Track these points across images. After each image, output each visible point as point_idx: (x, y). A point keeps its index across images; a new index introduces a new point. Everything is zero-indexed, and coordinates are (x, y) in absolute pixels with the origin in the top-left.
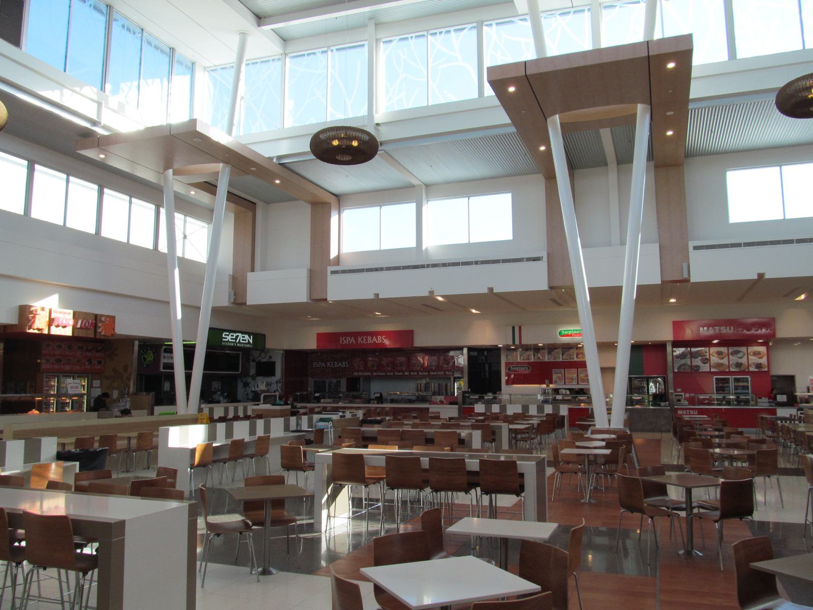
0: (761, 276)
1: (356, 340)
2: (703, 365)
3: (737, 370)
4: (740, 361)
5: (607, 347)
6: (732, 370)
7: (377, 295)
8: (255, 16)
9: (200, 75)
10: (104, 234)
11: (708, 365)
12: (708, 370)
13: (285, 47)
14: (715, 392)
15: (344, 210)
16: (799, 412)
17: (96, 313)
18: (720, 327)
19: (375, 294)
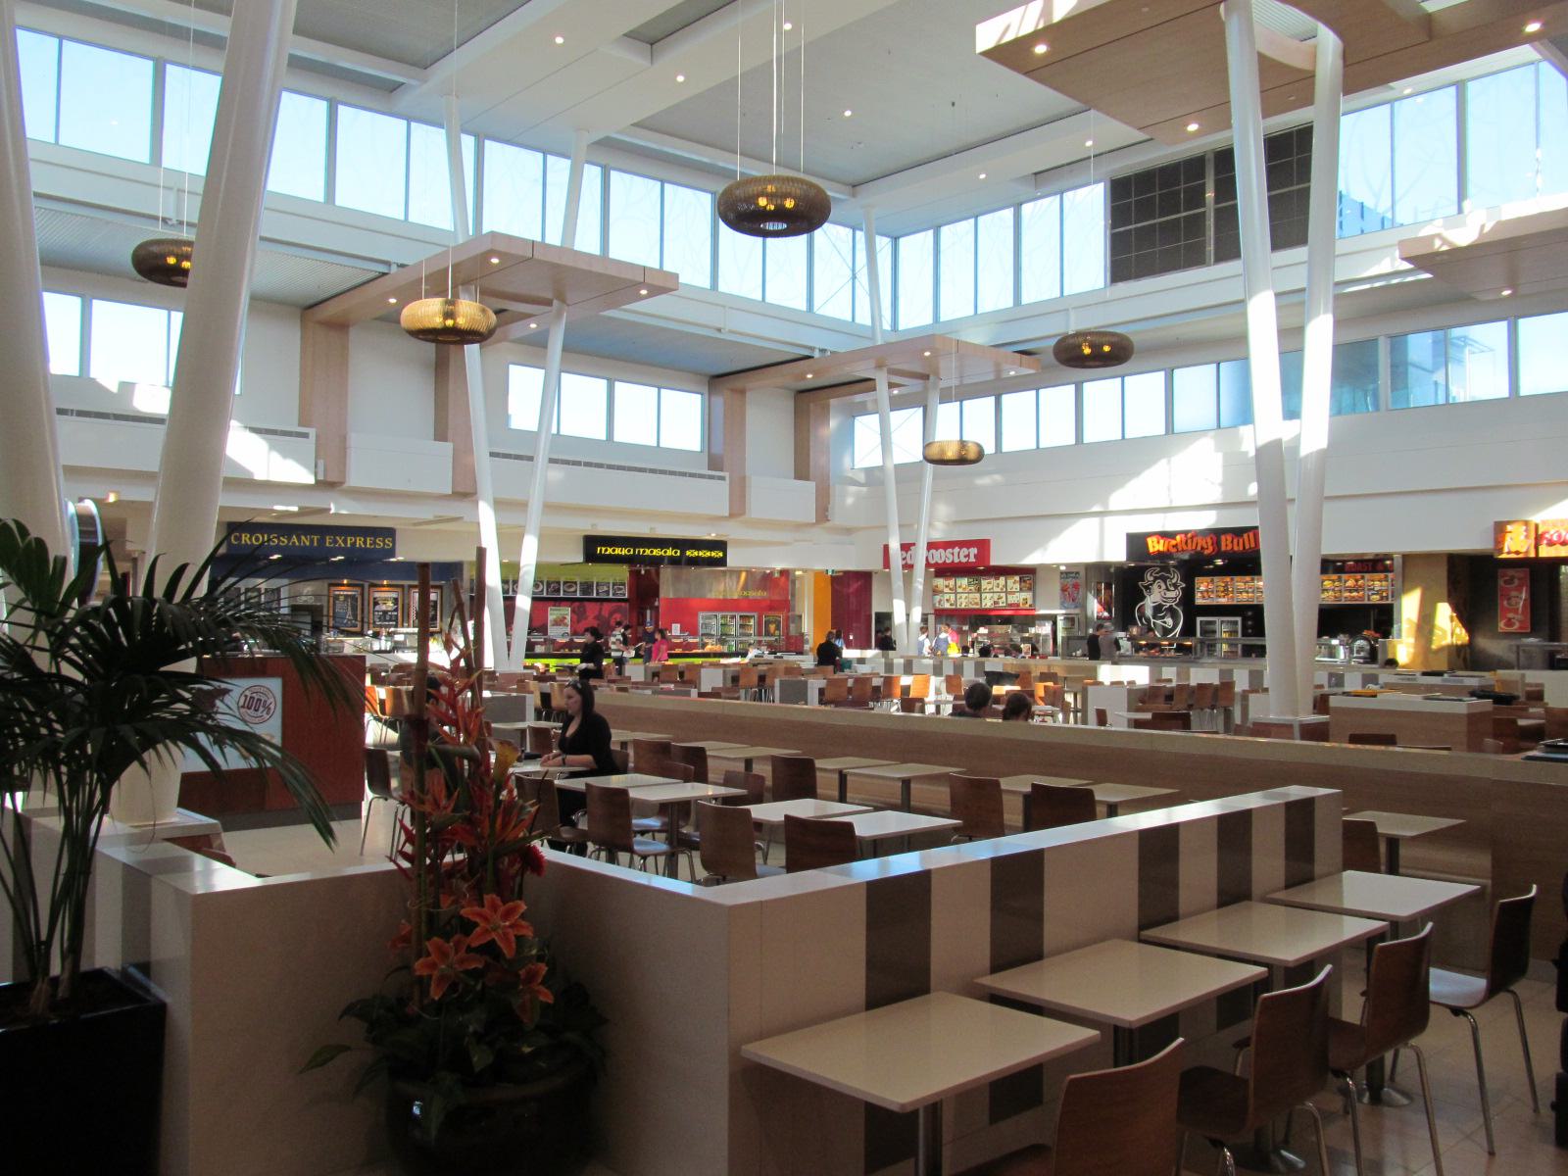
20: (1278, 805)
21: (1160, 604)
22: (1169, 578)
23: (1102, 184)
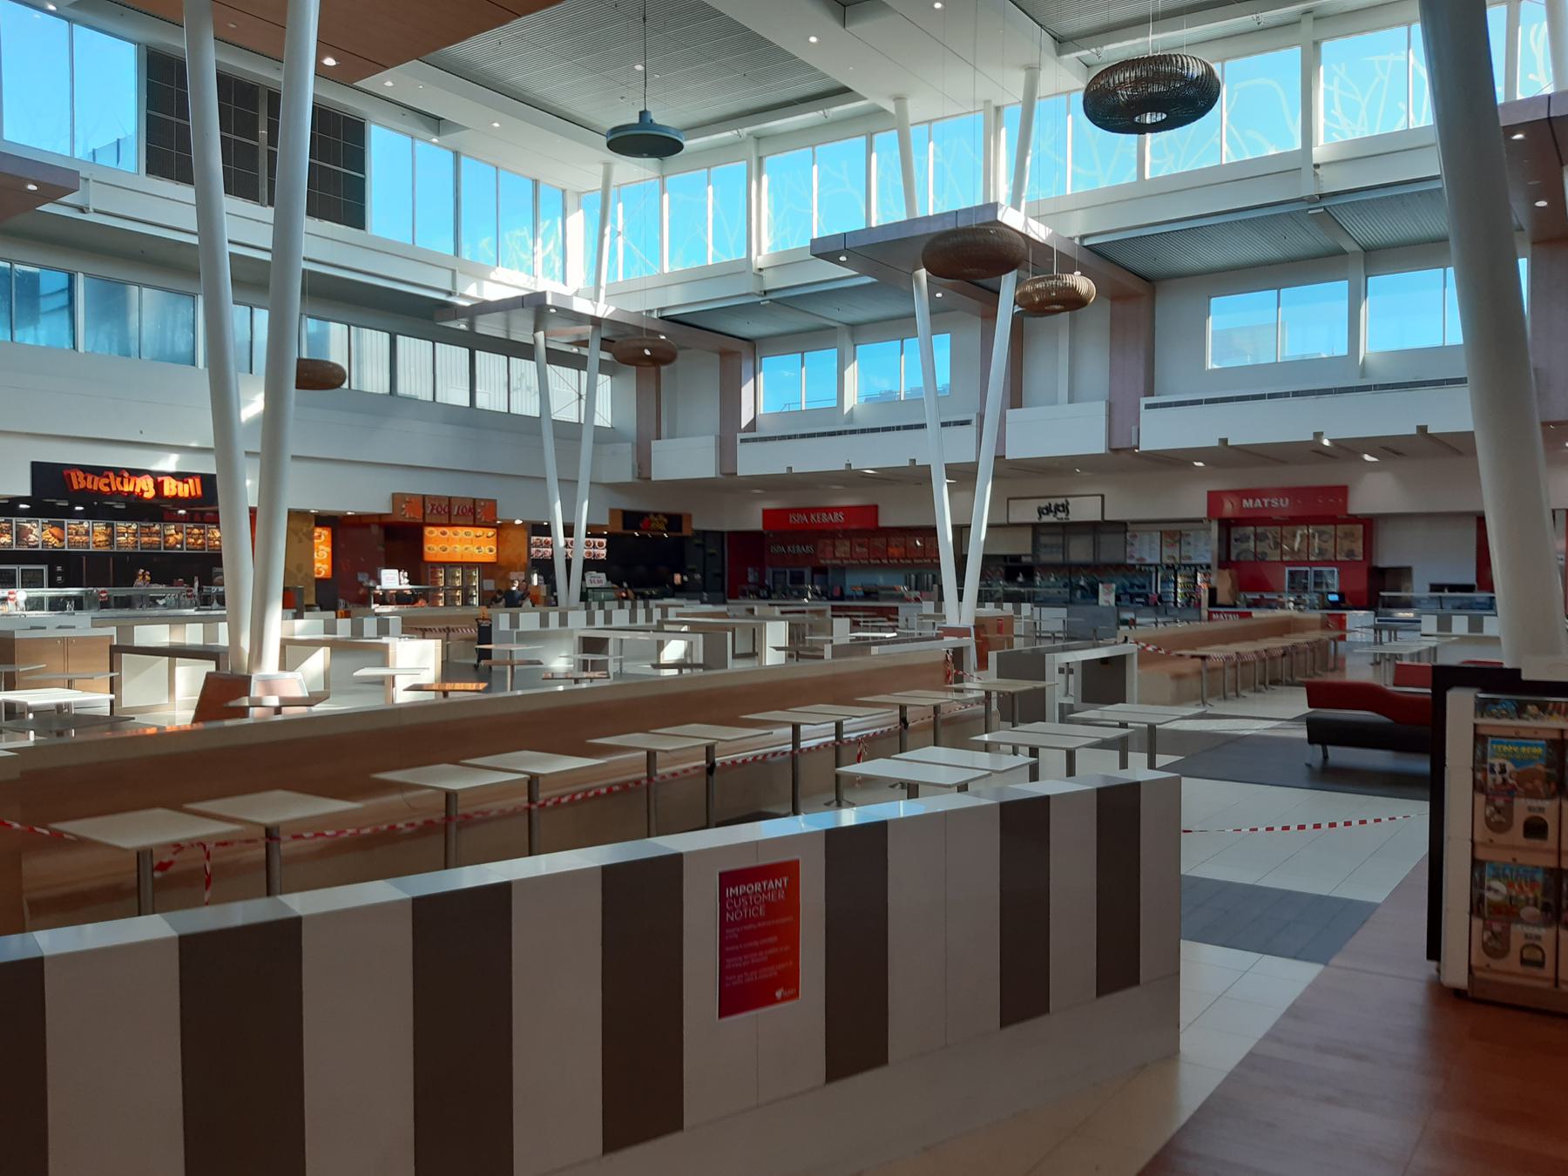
0: (1422, 429)
1: (809, 518)
3: (1319, 559)
12: (1279, 559)
14: (1287, 589)
15: (761, 358)
16: (1376, 619)
17: (474, 497)
18: (1271, 498)
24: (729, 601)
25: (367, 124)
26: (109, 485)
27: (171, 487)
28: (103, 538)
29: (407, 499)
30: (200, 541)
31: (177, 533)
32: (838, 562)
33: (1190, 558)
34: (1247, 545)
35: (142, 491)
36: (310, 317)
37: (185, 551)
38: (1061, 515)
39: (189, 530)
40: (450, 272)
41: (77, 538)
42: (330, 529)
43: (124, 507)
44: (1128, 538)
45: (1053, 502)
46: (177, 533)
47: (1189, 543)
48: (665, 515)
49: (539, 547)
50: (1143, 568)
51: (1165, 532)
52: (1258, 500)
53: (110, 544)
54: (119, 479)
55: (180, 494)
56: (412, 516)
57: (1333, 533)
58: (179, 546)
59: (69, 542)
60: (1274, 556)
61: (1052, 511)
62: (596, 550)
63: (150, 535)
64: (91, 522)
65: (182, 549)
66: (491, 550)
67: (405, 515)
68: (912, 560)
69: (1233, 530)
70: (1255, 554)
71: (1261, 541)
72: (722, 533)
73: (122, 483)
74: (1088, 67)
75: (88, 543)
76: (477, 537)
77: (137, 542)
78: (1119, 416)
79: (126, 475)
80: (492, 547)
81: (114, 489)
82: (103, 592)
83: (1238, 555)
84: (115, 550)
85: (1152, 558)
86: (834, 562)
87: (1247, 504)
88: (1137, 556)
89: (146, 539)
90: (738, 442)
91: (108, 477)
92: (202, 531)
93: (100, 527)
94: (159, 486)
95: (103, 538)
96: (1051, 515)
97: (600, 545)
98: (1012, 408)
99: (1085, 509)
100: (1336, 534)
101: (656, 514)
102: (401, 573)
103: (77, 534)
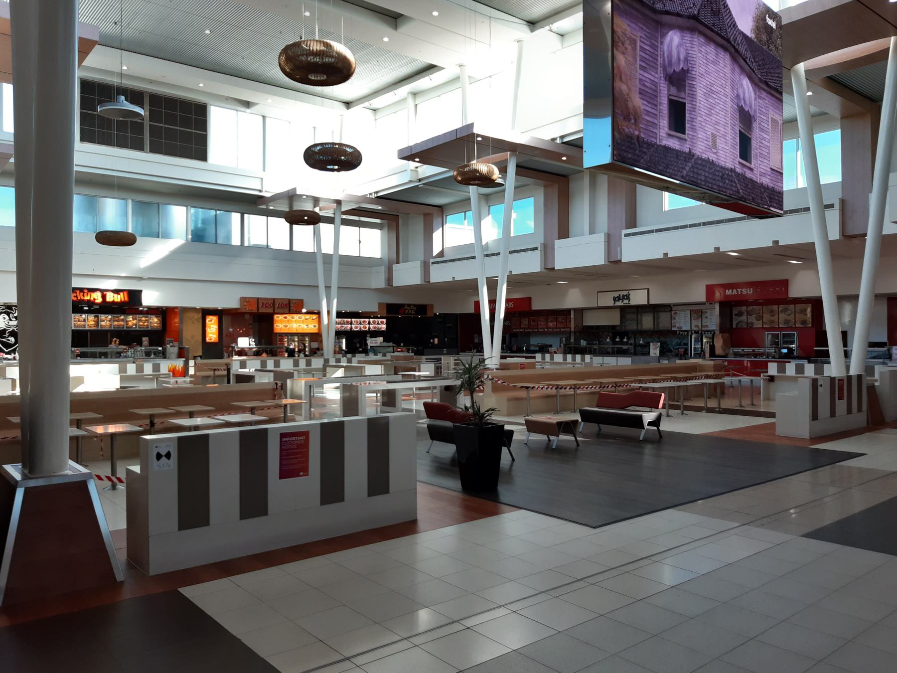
0: (776, 242)
2: (756, 321)
4: (788, 318)
5: (847, 299)
6: (781, 326)
7: (666, 254)
8: (343, 103)
9: (416, 103)
10: (295, 248)
11: (761, 322)
13: (375, 114)
15: (446, 216)
19: (774, 242)
20: (175, 437)
21: (5, 329)
22: (12, 313)
23: (637, 185)
24: (460, 353)
25: (208, 106)
26: (76, 297)
27: (110, 297)
28: (93, 323)
29: (248, 300)
30: (146, 324)
31: (133, 320)
32: (522, 330)
33: (707, 326)
34: (743, 319)
35: (94, 299)
36: (192, 207)
37: (138, 329)
38: (626, 301)
39: (140, 318)
40: (260, 179)
41: (79, 323)
42: (217, 316)
43: (98, 307)
44: (672, 314)
45: (622, 293)
46: (133, 320)
47: (707, 318)
48: (415, 305)
49: (342, 324)
50: (681, 333)
51: (693, 310)
52: (735, 290)
53: (97, 326)
54: (82, 294)
55: (116, 300)
56: (250, 309)
57: (793, 310)
58: (134, 326)
59: (74, 325)
60: (758, 324)
61: (621, 299)
62: (379, 326)
63: (117, 321)
64: (86, 315)
65: (136, 328)
66: (315, 326)
67: (246, 308)
68: (533, 329)
69: (734, 309)
70: (747, 323)
71: (750, 315)
72: (457, 314)
73: (83, 296)
74: (562, 36)
75: (84, 325)
76: (306, 319)
77: (111, 325)
78: (611, 243)
79: (86, 291)
80: (316, 325)
81: (79, 298)
82: (77, 350)
83: (737, 324)
84: (99, 328)
85: (686, 327)
86: (520, 330)
87: (729, 292)
88: (677, 325)
89: (116, 323)
90: (431, 264)
91: (76, 293)
92: (147, 319)
93: (91, 317)
94: (104, 297)
95: (93, 323)
96: (621, 301)
97: (382, 322)
98: (560, 238)
99: (638, 298)
100: (795, 311)
101: (409, 305)
102: (251, 339)
103: (79, 321)
